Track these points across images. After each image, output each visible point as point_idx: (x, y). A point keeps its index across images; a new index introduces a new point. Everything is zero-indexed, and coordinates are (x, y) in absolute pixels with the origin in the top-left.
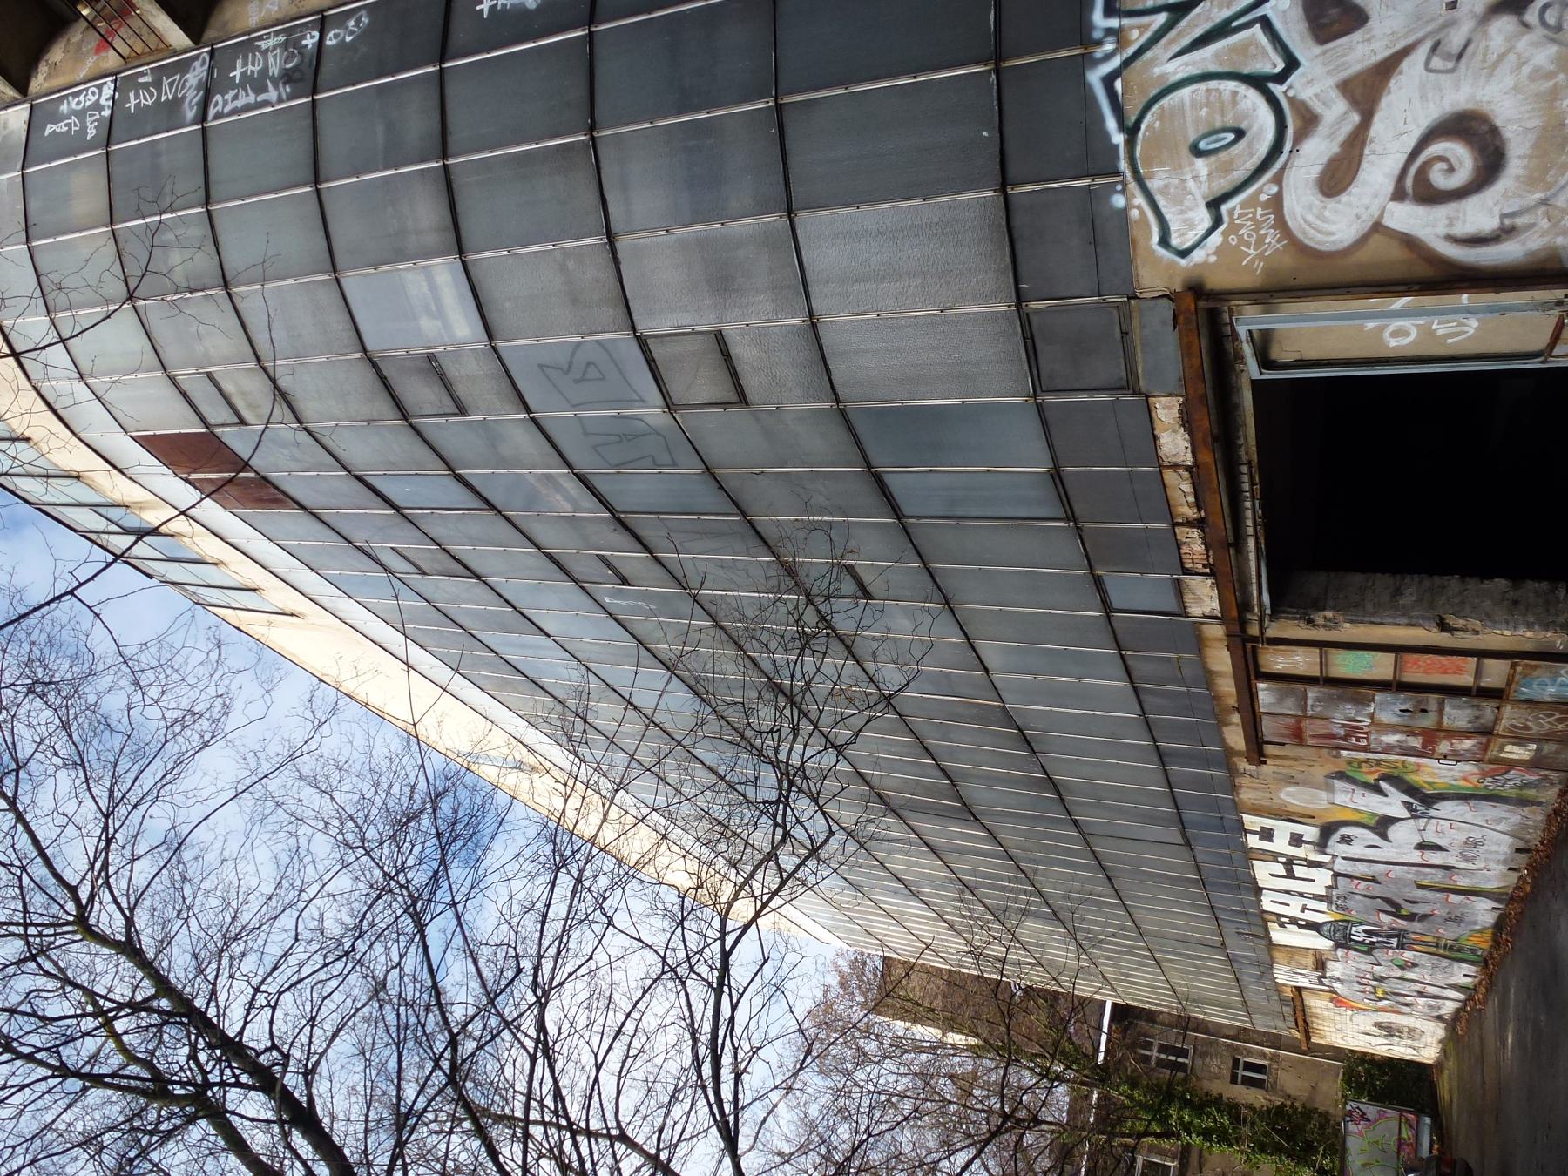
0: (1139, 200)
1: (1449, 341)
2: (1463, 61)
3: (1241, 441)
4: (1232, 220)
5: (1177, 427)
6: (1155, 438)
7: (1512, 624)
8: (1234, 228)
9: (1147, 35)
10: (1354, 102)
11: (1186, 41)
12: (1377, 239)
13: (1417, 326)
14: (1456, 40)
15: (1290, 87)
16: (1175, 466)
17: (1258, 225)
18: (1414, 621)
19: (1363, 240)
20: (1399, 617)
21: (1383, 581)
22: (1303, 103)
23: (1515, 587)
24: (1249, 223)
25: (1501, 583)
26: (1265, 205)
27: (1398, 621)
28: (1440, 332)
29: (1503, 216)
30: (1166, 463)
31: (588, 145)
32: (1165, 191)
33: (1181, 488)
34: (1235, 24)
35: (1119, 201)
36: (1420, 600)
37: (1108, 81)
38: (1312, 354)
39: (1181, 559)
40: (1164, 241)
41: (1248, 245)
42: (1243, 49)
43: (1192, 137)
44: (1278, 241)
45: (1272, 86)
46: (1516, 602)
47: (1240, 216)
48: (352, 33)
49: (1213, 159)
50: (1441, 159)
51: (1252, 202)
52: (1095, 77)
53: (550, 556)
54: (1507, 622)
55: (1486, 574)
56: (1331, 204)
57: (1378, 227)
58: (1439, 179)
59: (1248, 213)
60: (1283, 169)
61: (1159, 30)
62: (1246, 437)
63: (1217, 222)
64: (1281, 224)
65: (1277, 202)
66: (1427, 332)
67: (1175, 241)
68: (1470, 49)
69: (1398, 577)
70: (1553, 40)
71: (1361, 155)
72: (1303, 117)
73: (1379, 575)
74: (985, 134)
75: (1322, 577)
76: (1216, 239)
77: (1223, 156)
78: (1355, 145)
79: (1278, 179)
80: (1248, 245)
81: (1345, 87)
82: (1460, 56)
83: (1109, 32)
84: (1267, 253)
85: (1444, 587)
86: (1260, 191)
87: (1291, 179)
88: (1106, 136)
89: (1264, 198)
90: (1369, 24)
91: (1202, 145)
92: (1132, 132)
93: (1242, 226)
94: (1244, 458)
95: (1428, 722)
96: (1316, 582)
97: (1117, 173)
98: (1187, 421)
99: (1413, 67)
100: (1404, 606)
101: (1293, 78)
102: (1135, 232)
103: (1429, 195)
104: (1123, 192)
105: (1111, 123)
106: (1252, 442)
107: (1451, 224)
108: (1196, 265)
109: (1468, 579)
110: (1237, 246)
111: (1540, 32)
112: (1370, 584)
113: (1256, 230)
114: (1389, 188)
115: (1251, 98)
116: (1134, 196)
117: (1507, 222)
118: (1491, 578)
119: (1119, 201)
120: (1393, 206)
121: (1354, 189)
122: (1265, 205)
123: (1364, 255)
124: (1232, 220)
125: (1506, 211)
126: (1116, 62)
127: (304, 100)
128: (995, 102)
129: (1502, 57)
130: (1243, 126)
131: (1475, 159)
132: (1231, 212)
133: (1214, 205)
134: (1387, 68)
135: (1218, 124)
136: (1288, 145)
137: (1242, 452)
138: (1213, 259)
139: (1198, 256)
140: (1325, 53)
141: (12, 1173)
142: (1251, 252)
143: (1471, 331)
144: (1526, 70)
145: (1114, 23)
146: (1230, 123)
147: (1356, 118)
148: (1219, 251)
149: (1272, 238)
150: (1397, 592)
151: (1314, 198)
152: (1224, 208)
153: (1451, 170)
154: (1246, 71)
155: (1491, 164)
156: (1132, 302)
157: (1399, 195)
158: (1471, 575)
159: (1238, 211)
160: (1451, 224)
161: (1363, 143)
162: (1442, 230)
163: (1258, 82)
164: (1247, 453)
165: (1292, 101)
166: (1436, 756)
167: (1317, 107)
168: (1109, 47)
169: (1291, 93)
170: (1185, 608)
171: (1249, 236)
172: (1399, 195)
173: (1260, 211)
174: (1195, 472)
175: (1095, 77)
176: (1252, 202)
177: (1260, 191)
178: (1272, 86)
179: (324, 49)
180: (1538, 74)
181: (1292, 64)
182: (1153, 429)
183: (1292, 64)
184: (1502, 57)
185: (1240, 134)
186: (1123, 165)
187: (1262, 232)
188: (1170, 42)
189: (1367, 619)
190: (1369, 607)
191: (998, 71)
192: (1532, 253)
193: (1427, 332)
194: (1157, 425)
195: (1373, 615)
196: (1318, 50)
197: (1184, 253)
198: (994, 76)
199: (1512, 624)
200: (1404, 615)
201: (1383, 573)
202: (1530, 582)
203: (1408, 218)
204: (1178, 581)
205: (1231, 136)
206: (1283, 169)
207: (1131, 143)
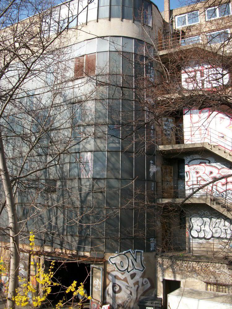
152: (114, 265)
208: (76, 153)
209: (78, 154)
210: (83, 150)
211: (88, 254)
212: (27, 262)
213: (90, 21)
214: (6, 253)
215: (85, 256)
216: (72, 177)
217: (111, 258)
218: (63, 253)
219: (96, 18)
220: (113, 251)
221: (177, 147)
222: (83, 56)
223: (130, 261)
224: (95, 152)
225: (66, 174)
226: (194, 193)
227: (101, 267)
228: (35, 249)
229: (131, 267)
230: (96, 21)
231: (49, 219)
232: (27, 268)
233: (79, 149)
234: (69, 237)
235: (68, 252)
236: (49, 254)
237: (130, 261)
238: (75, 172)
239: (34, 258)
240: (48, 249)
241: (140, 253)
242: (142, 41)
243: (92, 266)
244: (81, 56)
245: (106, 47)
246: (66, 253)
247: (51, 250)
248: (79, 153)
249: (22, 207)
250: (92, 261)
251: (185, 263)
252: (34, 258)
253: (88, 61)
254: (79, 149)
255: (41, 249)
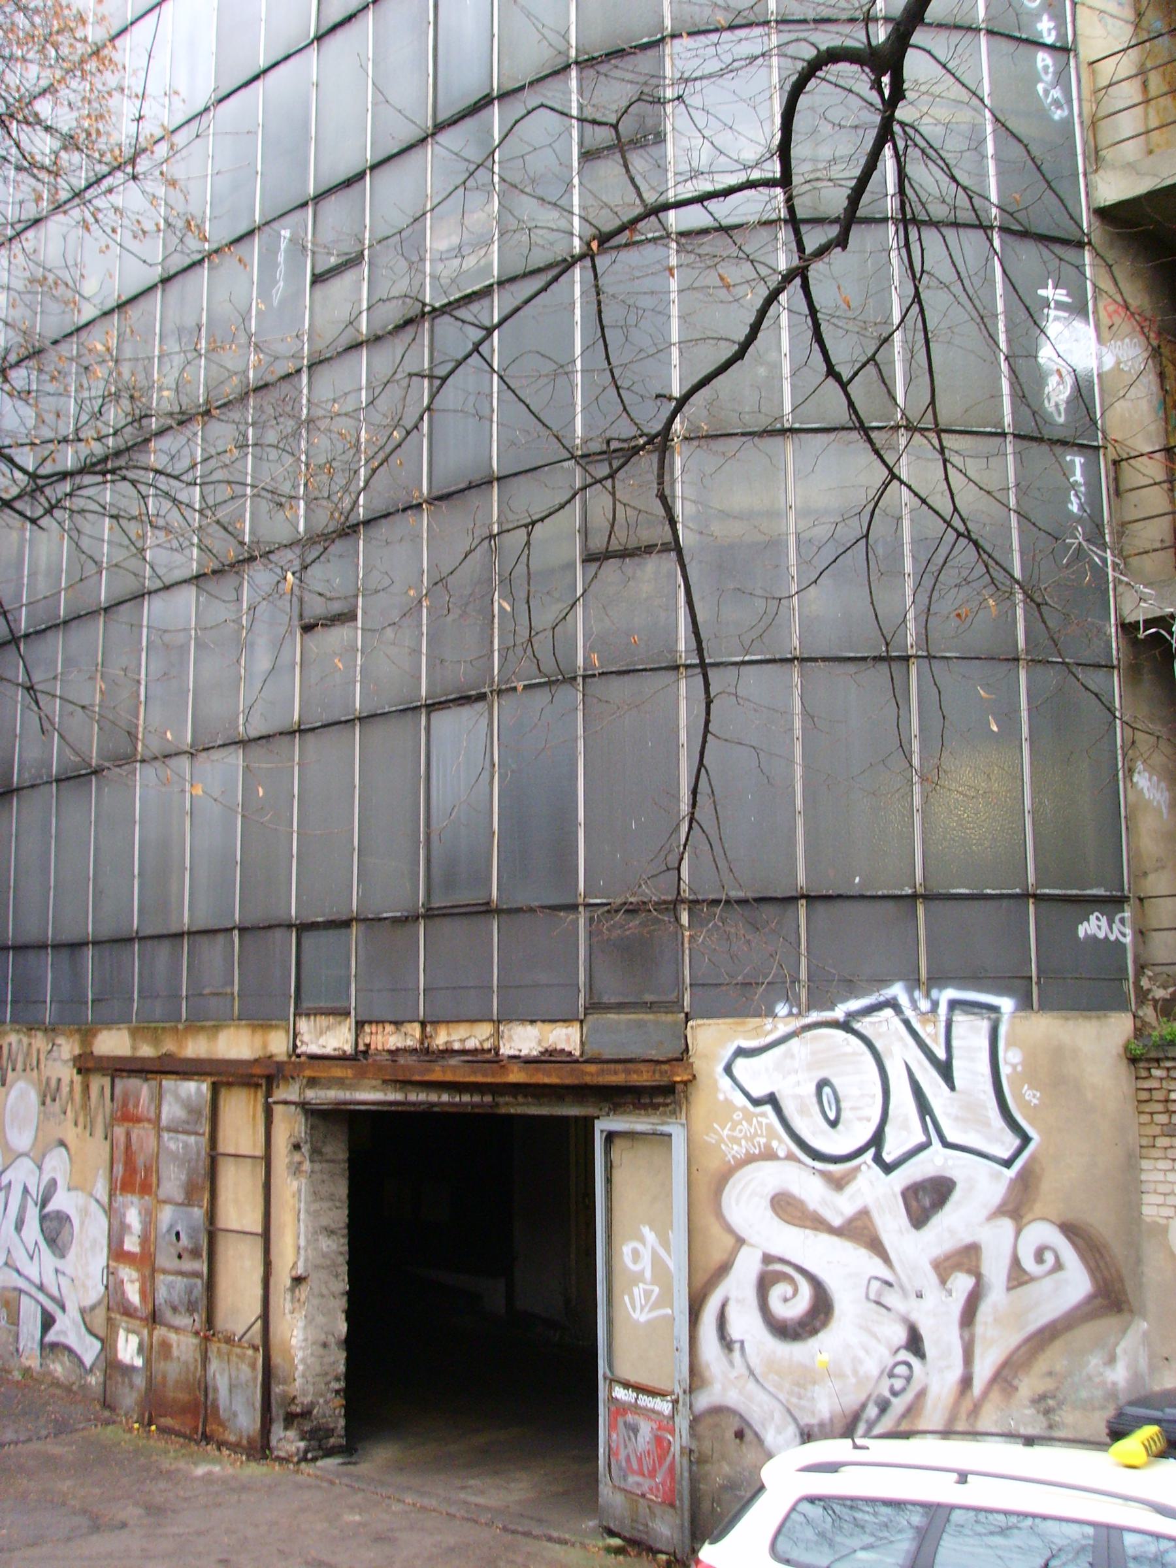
0: (782, 1029)
1: (626, 1298)
2: (874, 1306)
3: (521, 1099)
4: (757, 1115)
5: (546, 1045)
6: (532, 1022)
7: (303, 1344)
8: (748, 1117)
9: (928, 1041)
10: (850, 1221)
11: (919, 1077)
12: (729, 1241)
13: (642, 1272)
14: (892, 1298)
15: (869, 1167)
16: (498, 1035)
17: (750, 1139)
18: (302, 1252)
19: (729, 1229)
20: (306, 1237)
21: (339, 1217)
22: (854, 1178)
23: (338, 1343)
24: (752, 1131)
25: (342, 1328)
26: (768, 1146)
27: (302, 1237)
28: (636, 1290)
29: (742, 1343)
30: (501, 1028)
31: (889, 420)
32: (790, 1055)
33: (475, 1036)
34: (928, 1118)
35: (782, 1009)
36: (324, 1256)
37: (893, 1004)
38: (617, 1176)
39: (377, 1022)
40: (741, 1052)
41: (733, 1129)
42: (905, 1126)
43: (834, 1081)
44: (734, 1157)
45: (872, 1151)
46: (325, 1345)
47: (760, 1124)
48: (1047, 92)
49: (814, 1100)
50: (796, 1291)
51: (771, 1134)
52: (897, 990)
53: (360, 176)
54: (306, 1340)
55: (351, 1315)
56: (766, 1203)
57: (740, 1241)
58: (777, 1292)
59: (761, 1129)
60: (799, 1161)
61: (932, 1052)
62: (528, 1104)
63: (756, 1102)
64: (750, 1159)
65: (769, 1155)
66: (638, 1278)
67: (740, 1065)
68: (884, 1311)
69: (346, 1231)
70: (882, 1372)
71: (805, 1227)
72: (842, 1178)
73: (347, 1212)
74: (857, 880)
75: (343, 1155)
76: (740, 1100)
77: (816, 1109)
78: (818, 1223)
79: (790, 1157)
80: (733, 1129)
81: (864, 1213)
82: (878, 1303)
83: (935, 1005)
84: (723, 1147)
85: (337, 1276)
86: (781, 1141)
87: (791, 1166)
88: (844, 1000)
89: (775, 1144)
90: (913, 1230)
91: (827, 1090)
92: (845, 1026)
93: (750, 1124)
94: (501, 1100)
95: (165, 1260)
96: (338, 1150)
97: (809, 1009)
98: (550, 1057)
99: (876, 1266)
100: (317, 1240)
101: (876, 1169)
102: (753, 1022)
103: (764, 1285)
104: (790, 1014)
105: (855, 1005)
106: (520, 1110)
107: (738, 1301)
108: (716, 1082)
109: (345, 1299)
110: (732, 1120)
111: (890, 1362)
112: (338, 1204)
113: (745, 1137)
114: (775, 1251)
115: (865, 1133)
116: (786, 1025)
117: (737, 1346)
118: (347, 1319)
119: (782, 1009)
120: (758, 1256)
121: (776, 1221)
122: (768, 1146)
123: (716, 1229)
124: (757, 1115)
125: (746, 1345)
126: (909, 1013)
127: (1008, 419)
128: (886, 892)
129: (874, 1335)
130: (840, 1127)
131: (792, 1319)
132: (764, 1115)
133: (772, 1100)
134: (876, 1246)
135: (843, 1105)
136: (819, 1165)
137: (507, 1099)
138: (721, 1097)
139: (725, 1082)
140: (895, 1196)
141: (3, 122)
142: (726, 1132)
143: (635, 1316)
144: (861, 1354)
145: (943, 1009)
146: (845, 1115)
147: (837, 1222)
148: (728, 1102)
149: (737, 1151)
150: (330, 1232)
151: (771, 1189)
152: (768, 1109)
153: (786, 1300)
154: (888, 1129)
155: (785, 1331)
156: (682, 1015)
157: (768, 1259)
158: (349, 1301)
159: (764, 1121)
160: (738, 1301)
161: (815, 1229)
162: (733, 1295)
163: (877, 1140)
164: (507, 1104)
165: (857, 1169)
166: (113, 1264)
167: (850, 1189)
168: (925, 1005)
169: (864, 1167)
170: (308, 1015)
171: (741, 1131)
172: (768, 1259)
173: (763, 1140)
174: (489, 1058)
175: (897, 990)
176: (771, 1134)
177: (781, 1141)
178: (872, 1151)
179: (1031, 48)
180: (856, 1361)
181: (888, 1168)
182: (544, 1021)
183: (888, 1168)
184: (874, 1335)
185: (834, 1124)
186: (815, 1016)
187: (743, 1142)
188: (919, 1062)
189: (302, 1205)
190: (316, 1206)
191: (914, 897)
192: (708, 1366)
193: (638, 1278)
194: (547, 1027)
195: (307, 1211)
196: (898, 1189)
197: (728, 1070)
198: (910, 891)
199: (303, 1344)
200: (308, 1241)
201: (349, 1216)
202: (344, 1355)
203: (746, 1268)
204: (349, 1013)
205: (832, 1116)
206: (799, 1161)
207: (835, 1024)
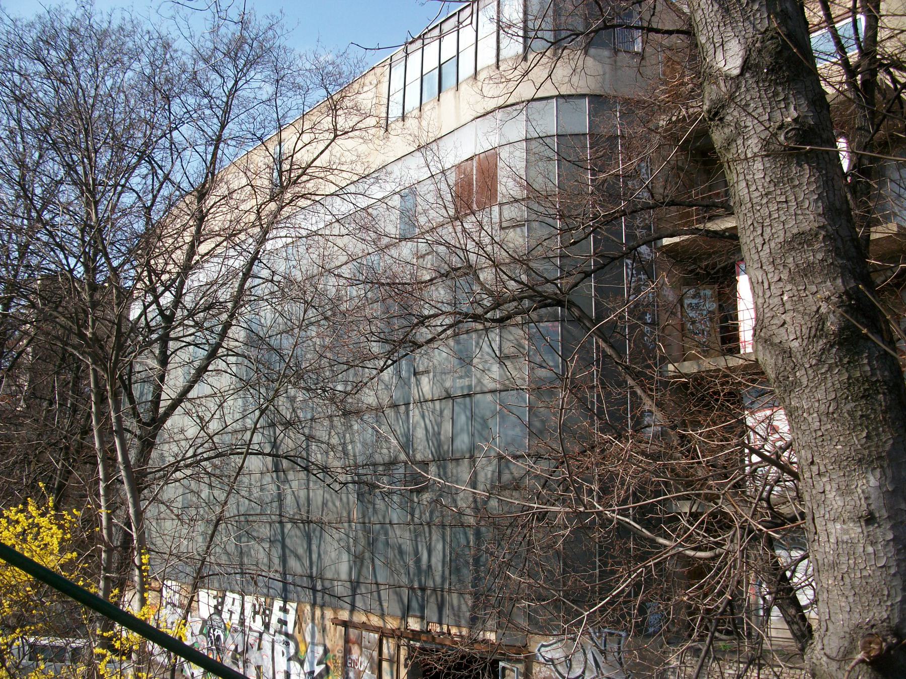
208: (464, 396)
209: (468, 399)
210: (478, 389)
211: (491, 636)
212: (375, 654)
213: (482, 69)
214: (338, 634)
215: (485, 641)
216: (458, 456)
217: (543, 646)
218: (444, 634)
219: (494, 61)
220: (545, 630)
221: (721, 363)
222: (471, 159)
223: (590, 657)
224: (503, 394)
225: (446, 447)
226: (136, 435)
227: (521, 667)
228: (392, 624)
229: (592, 671)
230: (494, 68)
231: (416, 552)
232: (375, 666)
233: (470, 387)
234: (455, 596)
235: (454, 631)
236: (415, 635)
237: (590, 657)
238: (463, 442)
239: (389, 647)
240: (414, 624)
241: (615, 638)
242: (601, 96)
243: (501, 664)
244: (467, 160)
245: (517, 130)
246: (449, 634)
247: (422, 625)
248: (469, 395)
249: (365, 527)
250: (501, 654)
251: (730, 668)
252: (389, 647)
253: (481, 171)
254: (470, 387)
255: (401, 623)
